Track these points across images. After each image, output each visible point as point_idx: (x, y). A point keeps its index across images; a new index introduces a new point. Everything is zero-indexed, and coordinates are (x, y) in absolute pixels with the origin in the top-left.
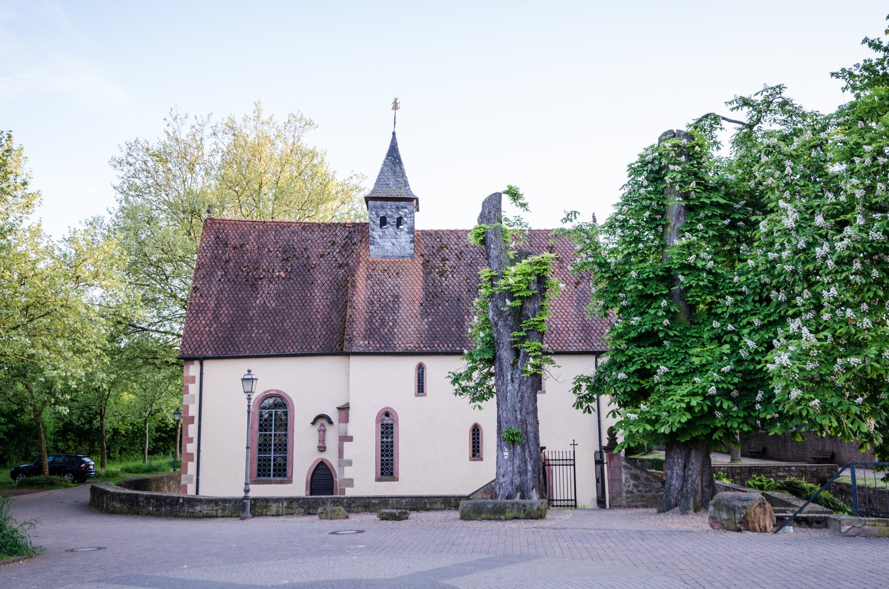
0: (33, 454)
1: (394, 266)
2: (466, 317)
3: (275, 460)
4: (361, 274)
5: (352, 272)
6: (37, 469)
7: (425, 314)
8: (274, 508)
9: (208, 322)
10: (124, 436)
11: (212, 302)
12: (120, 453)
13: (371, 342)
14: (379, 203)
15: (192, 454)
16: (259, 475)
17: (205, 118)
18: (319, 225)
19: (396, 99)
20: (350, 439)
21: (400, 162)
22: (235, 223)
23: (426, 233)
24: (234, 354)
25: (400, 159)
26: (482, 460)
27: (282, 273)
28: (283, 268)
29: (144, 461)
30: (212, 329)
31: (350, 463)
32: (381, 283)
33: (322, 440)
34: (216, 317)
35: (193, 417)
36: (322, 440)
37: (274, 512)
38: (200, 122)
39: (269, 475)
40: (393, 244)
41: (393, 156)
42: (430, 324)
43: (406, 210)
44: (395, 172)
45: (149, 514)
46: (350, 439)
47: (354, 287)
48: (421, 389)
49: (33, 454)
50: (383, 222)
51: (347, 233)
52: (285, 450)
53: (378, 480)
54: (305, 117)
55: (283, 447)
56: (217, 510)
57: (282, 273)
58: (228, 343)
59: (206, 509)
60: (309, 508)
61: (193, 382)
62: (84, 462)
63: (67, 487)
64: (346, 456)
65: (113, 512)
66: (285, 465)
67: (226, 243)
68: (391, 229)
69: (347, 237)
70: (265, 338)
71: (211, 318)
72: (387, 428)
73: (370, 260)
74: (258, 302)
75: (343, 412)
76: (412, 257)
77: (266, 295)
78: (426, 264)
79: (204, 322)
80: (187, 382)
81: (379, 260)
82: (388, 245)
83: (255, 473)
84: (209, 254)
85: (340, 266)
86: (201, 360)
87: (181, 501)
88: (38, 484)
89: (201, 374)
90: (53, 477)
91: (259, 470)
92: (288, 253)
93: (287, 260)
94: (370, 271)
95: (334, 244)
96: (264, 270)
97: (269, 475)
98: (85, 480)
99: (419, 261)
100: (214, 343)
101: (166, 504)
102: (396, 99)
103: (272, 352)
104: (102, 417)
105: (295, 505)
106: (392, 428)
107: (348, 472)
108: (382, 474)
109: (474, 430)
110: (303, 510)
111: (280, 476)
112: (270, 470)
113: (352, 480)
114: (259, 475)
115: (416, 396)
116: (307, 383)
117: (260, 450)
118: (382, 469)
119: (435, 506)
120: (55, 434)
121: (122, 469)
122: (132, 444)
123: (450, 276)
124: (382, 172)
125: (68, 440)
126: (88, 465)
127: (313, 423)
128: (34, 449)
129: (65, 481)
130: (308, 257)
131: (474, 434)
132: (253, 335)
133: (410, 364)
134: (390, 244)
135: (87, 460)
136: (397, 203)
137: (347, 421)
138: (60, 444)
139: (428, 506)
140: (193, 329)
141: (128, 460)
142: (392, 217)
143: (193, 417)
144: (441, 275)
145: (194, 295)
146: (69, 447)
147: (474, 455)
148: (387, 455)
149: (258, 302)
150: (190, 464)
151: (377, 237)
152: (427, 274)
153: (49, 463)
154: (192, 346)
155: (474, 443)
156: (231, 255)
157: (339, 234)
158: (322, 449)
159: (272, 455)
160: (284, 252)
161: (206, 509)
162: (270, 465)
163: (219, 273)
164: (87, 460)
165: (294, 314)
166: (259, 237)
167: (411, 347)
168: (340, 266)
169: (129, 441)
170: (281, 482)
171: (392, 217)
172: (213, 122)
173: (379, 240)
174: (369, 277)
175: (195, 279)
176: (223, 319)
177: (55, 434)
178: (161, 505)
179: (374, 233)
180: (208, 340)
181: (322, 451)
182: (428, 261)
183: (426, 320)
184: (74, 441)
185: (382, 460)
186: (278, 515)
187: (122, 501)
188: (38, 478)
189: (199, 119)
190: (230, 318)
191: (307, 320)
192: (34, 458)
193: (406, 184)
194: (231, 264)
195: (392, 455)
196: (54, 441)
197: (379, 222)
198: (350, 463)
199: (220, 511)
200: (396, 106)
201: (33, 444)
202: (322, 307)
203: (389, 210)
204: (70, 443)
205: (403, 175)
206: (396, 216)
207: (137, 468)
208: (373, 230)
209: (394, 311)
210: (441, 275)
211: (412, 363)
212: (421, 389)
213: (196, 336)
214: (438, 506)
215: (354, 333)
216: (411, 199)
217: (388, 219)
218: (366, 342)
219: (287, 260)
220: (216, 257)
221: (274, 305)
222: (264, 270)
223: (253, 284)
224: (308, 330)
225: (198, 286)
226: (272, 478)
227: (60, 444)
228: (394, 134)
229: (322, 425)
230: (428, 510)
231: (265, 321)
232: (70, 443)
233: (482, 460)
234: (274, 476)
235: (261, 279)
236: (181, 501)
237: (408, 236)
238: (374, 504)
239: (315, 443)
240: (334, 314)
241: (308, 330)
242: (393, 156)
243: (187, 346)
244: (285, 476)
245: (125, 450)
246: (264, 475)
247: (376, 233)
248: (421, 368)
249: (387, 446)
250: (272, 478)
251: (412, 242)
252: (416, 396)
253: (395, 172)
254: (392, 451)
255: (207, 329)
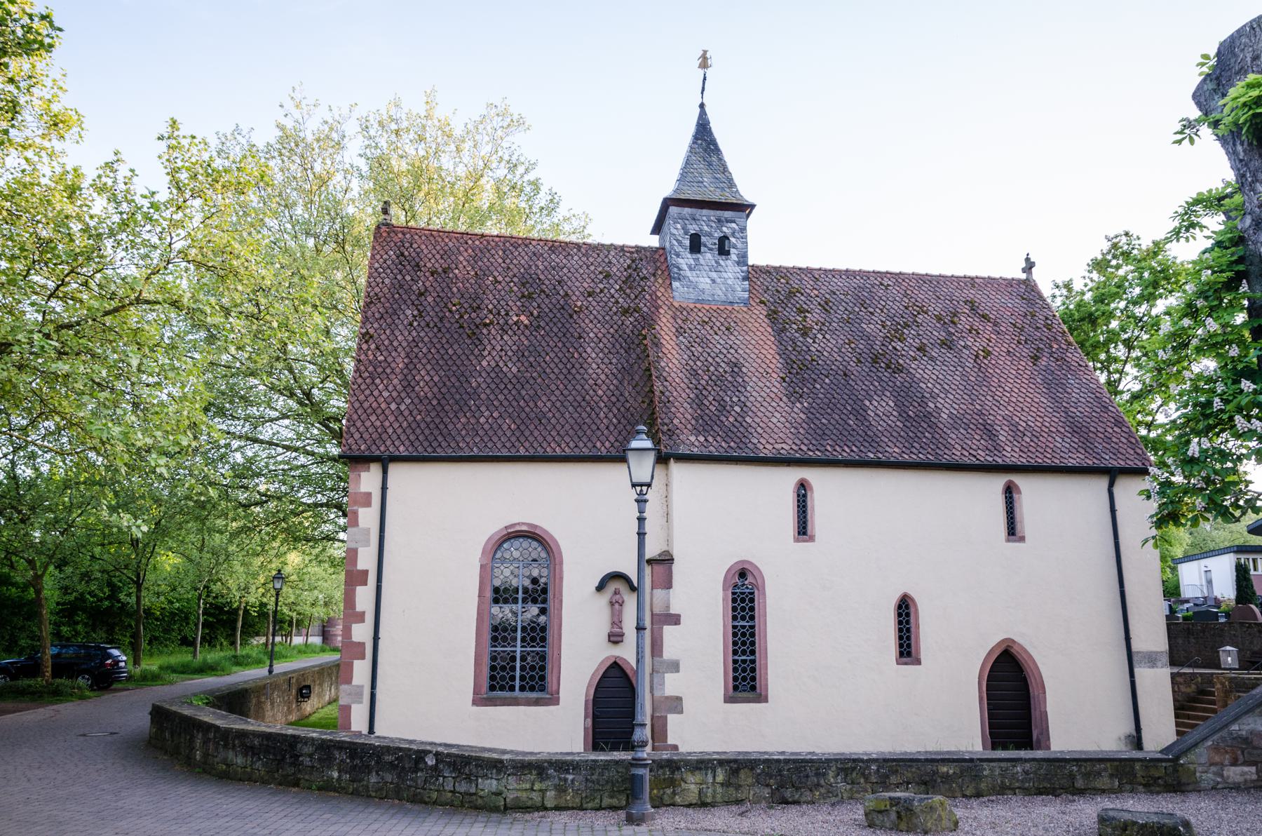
0: (22, 642)
1: (717, 317)
2: (867, 403)
3: (523, 659)
4: (665, 327)
5: (648, 321)
6: (33, 668)
7: (794, 395)
8: (692, 785)
9: (395, 394)
10: (157, 619)
11: (399, 360)
12: (150, 643)
13: (710, 439)
14: (687, 211)
15: (362, 645)
16: (492, 688)
17: (345, 111)
18: (578, 246)
19: (705, 52)
20: (675, 620)
21: (717, 150)
22: (433, 236)
23: (767, 271)
24: (450, 452)
25: (716, 145)
26: (918, 662)
27: (523, 318)
28: (523, 310)
29: (195, 656)
30: (403, 407)
31: (675, 667)
32: (704, 342)
33: (617, 621)
34: (408, 386)
35: (366, 573)
36: (617, 621)
37: (693, 797)
38: (337, 118)
39: (512, 689)
40: (714, 281)
41: (704, 137)
42: (807, 411)
43: (734, 225)
44: (710, 164)
45: (327, 788)
46: (675, 620)
47: (657, 344)
48: (803, 529)
49: (22, 642)
50: (696, 245)
51: (629, 262)
52: (543, 639)
53: (729, 699)
54: (511, 110)
55: (539, 635)
56: (543, 791)
57: (523, 318)
58: (436, 432)
59: (514, 788)
60: (781, 786)
61: (368, 504)
62: (110, 656)
63: (82, 698)
64: (669, 653)
65: (226, 777)
66: (543, 668)
67: (417, 265)
68: (709, 256)
69: (629, 267)
70: (505, 427)
71: (399, 388)
72: (744, 598)
73: (676, 305)
74: (484, 363)
75: (659, 569)
76: (746, 303)
77: (497, 353)
78: (772, 316)
79: (386, 394)
80: (356, 503)
81: (692, 306)
82: (704, 282)
83: (485, 683)
84: (387, 281)
85: (626, 312)
86: (385, 461)
87: (430, 761)
88: (33, 693)
89: (384, 488)
90: (58, 681)
91: (492, 678)
92: (530, 288)
93: (530, 297)
94: (680, 322)
95: (608, 276)
96: (491, 312)
97: (512, 689)
98: (110, 685)
99: (760, 312)
100: (409, 431)
101: (381, 766)
102: (705, 52)
103: (522, 452)
104: (139, 586)
105: (745, 777)
106: (752, 600)
107: (672, 685)
108: (735, 688)
109: (900, 607)
110: (766, 792)
111: (532, 689)
112: (513, 678)
113: (679, 699)
114: (492, 688)
115: (796, 540)
116: (584, 510)
117: (494, 639)
118: (735, 679)
119: (1098, 784)
120: (57, 614)
121: (161, 668)
122: (167, 631)
123: (820, 336)
124: (688, 163)
125: (77, 623)
126: (117, 662)
127: (600, 588)
128: (24, 635)
129: (79, 688)
130: (567, 294)
131: (900, 615)
132: (482, 420)
133: (779, 484)
134: (703, 281)
135: (115, 652)
136: (719, 213)
137: (668, 585)
138: (64, 629)
139: (1080, 783)
140: (366, 405)
141: (161, 653)
142: (710, 235)
143: (366, 573)
144: (805, 334)
145: (365, 346)
146: (77, 633)
147: (901, 654)
148: (744, 652)
149: (484, 363)
150: (356, 663)
151: (685, 267)
152: (780, 332)
153: (53, 657)
154: (366, 436)
155: (900, 630)
156: (428, 284)
157: (614, 261)
158: (615, 638)
159: (519, 649)
160: (523, 285)
161: (514, 788)
162: (513, 669)
163: (408, 312)
164: (115, 652)
165: (553, 387)
166: (475, 259)
167: (785, 449)
168: (626, 312)
169: (171, 627)
170: (537, 703)
171: (710, 235)
172: (360, 112)
173: (688, 273)
174: (680, 332)
175: (365, 320)
176: (422, 389)
177: (57, 614)
178: (367, 769)
179: (680, 260)
180: (396, 425)
181: (616, 643)
182: (775, 312)
183: (798, 405)
184: (86, 625)
185: (735, 662)
186: (702, 804)
187: (249, 750)
188: (32, 682)
189: (336, 111)
190: (435, 390)
191: (579, 398)
192: (22, 650)
193: (731, 184)
194: (430, 299)
195: (753, 652)
196: (55, 624)
197: (687, 243)
198: (675, 667)
199: (550, 794)
200: (704, 63)
201: (22, 628)
202: (603, 377)
203: (705, 222)
204: (79, 627)
205: (725, 169)
206: (717, 235)
207: (183, 666)
208: (678, 255)
209: (739, 388)
210: (805, 334)
211: (788, 478)
212: (803, 529)
213: (373, 418)
214: (1104, 782)
215: (676, 421)
216: (744, 208)
217: (703, 239)
218: (702, 439)
219: (530, 297)
220: (401, 286)
221: (514, 370)
222: (491, 312)
223: (474, 334)
224: (584, 415)
225: (372, 331)
226: (517, 693)
227: (64, 629)
228: (702, 106)
229: (616, 592)
230: (1081, 792)
231: (501, 397)
232: (79, 627)
233: (918, 662)
234: (522, 689)
235: (486, 325)
236: (430, 761)
237: (737, 269)
238: (946, 778)
239: (605, 628)
240: (628, 391)
241: (584, 415)
242: (704, 137)
243: (357, 436)
244: (542, 689)
245: (156, 638)
246: (502, 688)
247: (685, 260)
248: (803, 490)
249: (744, 635)
250: (517, 693)
251: (744, 279)
252: (796, 540)
253: (710, 164)
254: (753, 643)
255: (393, 406)
